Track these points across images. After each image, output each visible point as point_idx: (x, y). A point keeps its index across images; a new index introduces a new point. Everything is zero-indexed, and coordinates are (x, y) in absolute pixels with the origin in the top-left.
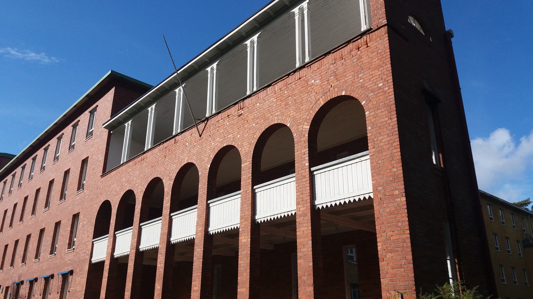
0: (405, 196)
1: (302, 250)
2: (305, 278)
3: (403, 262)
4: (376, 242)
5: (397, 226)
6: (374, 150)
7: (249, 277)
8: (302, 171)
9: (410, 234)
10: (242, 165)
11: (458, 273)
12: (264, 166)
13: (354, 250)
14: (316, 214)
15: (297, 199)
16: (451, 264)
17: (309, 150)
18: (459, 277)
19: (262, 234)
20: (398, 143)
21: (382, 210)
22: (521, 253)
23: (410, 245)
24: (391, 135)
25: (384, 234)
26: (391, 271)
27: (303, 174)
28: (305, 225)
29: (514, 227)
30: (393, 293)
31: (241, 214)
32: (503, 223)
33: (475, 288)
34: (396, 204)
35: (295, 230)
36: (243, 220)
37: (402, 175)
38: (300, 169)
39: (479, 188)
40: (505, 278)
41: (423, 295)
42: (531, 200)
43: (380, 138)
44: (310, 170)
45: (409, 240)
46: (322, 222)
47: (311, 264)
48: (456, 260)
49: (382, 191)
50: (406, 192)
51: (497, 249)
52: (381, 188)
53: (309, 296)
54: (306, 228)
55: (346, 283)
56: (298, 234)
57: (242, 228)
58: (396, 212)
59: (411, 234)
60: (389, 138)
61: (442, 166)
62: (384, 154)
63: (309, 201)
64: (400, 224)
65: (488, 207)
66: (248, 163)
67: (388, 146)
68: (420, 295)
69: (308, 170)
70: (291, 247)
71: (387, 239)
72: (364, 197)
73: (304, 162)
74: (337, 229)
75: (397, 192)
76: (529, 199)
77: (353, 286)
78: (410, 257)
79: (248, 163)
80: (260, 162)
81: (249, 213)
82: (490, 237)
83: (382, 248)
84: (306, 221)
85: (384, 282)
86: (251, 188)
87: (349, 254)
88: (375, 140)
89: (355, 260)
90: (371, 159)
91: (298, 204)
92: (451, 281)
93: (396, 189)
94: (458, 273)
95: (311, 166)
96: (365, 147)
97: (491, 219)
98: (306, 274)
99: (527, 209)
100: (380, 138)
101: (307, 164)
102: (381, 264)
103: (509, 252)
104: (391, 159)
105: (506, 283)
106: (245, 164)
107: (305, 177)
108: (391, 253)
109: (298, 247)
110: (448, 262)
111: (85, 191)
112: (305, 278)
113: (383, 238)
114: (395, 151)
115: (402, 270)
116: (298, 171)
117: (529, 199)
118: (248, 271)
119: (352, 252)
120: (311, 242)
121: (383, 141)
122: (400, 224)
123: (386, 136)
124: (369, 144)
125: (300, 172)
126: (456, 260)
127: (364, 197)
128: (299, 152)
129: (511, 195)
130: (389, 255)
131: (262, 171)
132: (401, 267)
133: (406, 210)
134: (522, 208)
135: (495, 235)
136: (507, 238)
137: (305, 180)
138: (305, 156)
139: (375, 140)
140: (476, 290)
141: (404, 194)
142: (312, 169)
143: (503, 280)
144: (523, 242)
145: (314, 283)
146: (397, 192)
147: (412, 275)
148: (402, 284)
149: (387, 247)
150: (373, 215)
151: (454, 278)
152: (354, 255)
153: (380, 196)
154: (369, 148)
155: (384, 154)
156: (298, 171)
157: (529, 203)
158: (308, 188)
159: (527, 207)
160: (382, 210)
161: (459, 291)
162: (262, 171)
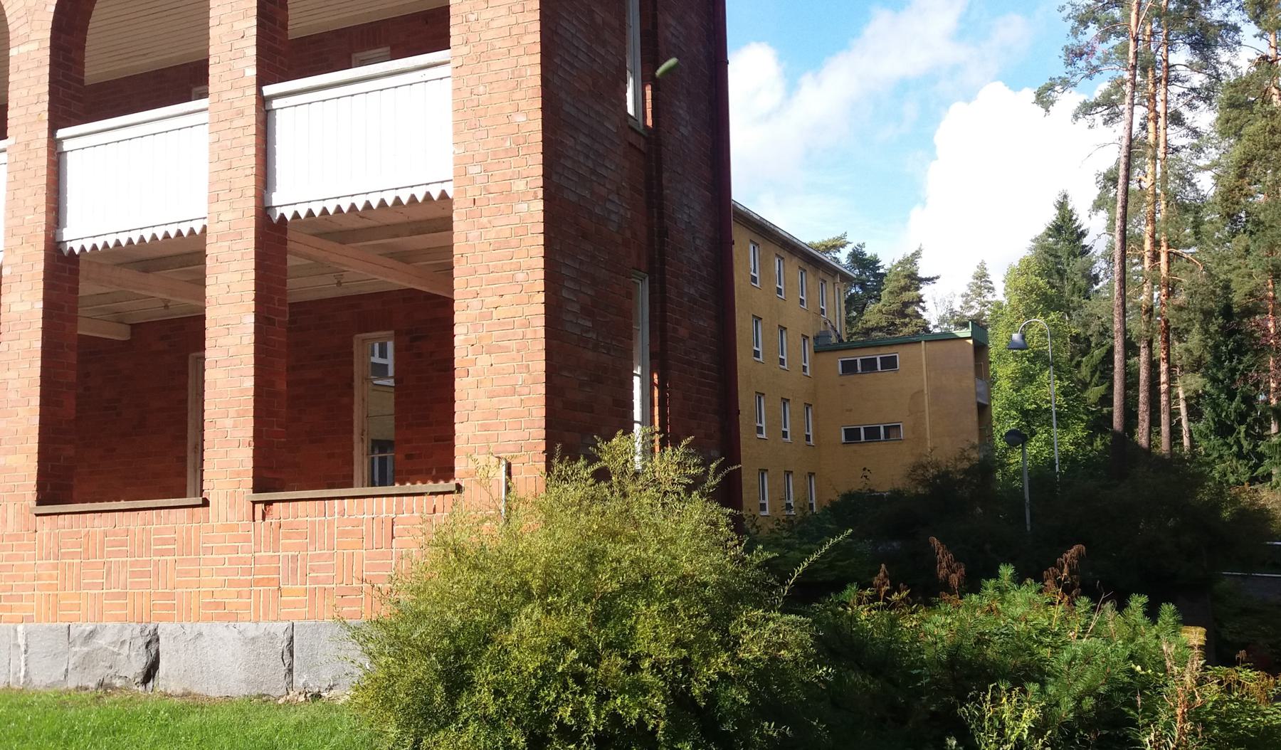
0: (544, 199)
1: (221, 341)
2: (228, 423)
3: (520, 378)
4: (452, 325)
5: (513, 280)
6: (465, 50)
7: (36, 420)
8: (231, 95)
9: (546, 303)
10: (13, 52)
11: (656, 409)
12: (99, 64)
13: (390, 346)
14: (273, 235)
15: (211, 183)
16: (642, 388)
17: (258, 26)
18: (657, 418)
19: (86, 288)
20: (537, 38)
21: (475, 233)
22: (807, 365)
23: (541, 332)
24: (518, 8)
25: (475, 303)
26: (483, 401)
27: (237, 104)
28: (234, 266)
29: (802, 301)
30: (482, 460)
31: (6, 220)
32: (779, 291)
33: (684, 443)
34: (515, 219)
35: (200, 282)
36: (17, 241)
37: (539, 137)
38: (226, 86)
39: (733, 197)
40: (763, 425)
41: (561, 462)
42: (848, 239)
43: (487, 15)
44: (259, 92)
45: (541, 321)
46: (292, 261)
47: (249, 383)
48: (656, 376)
49: (479, 179)
50: (545, 188)
51: (757, 354)
52: (477, 169)
53: (239, 474)
54: (237, 276)
55: (356, 437)
56: (209, 292)
57: (12, 266)
58: (514, 242)
59: (547, 304)
60: (512, 20)
61: (649, 123)
62: (496, 66)
63: (252, 192)
64: (520, 276)
65: (751, 247)
66: (34, 46)
67: (508, 43)
68: (555, 461)
69: (254, 91)
70: (188, 333)
71: (483, 317)
72: (428, 194)
73: (239, 64)
74: (339, 284)
75: (520, 185)
76: (845, 234)
77: (380, 445)
78: (540, 366)
79: (34, 46)
80: (83, 48)
81: (37, 220)
82: (743, 324)
83: (466, 340)
84: (238, 255)
85: (462, 431)
86: (45, 134)
87: (376, 359)
88: (472, 18)
89: (391, 372)
90: (456, 78)
91: (214, 198)
92: (637, 426)
93: (521, 177)
94: (656, 409)
95: (262, 80)
96: (442, 42)
97: (754, 279)
98: (232, 412)
99: (838, 261)
100: (487, 15)
101: (252, 72)
102: (459, 383)
103: (782, 362)
104: (512, 84)
105: (764, 436)
106: (23, 49)
107: (241, 113)
108: (489, 353)
109: (208, 334)
110: (637, 381)
111: (909, 460)
112: (228, 423)
113: (473, 312)
114: (526, 60)
115: (516, 398)
116: (219, 93)
117: (845, 234)
118: (36, 401)
119: (383, 354)
120: (250, 319)
121: (494, 24)
122: (520, 276)
123: (504, 11)
124: (453, 31)
125: (225, 96)
126: (656, 376)
127: (428, 194)
128: (224, 29)
129: (802, 221)
130: (484, 360)
131: (88, 82)
132: (514, 392)
133: (542, 237)
134: (827, 258)
135: (758, 319)
136: (783, 329)
137: (238, 123)
138: (243, 43)
139: (472, 18)
140: (687, 446)
141: (540, 193)
142: (268, 90)
143: (760, 430)
144: (816, 338)
145: (255, 437)
146: (520, 185)
147: (539, 412)
148: (512, 435)
149: (480, 339)
150: (450, 248)
151: (647, 420)
152: (390, 361)
153: (472, 192)
154: (453, 41)
155: (496, 66)
156: (219, 93)
157: (843, 246)
158: (253, 151)
159: (838, 255)
160: (475, 233)
161: (653, 450)
162: (88, 82)
